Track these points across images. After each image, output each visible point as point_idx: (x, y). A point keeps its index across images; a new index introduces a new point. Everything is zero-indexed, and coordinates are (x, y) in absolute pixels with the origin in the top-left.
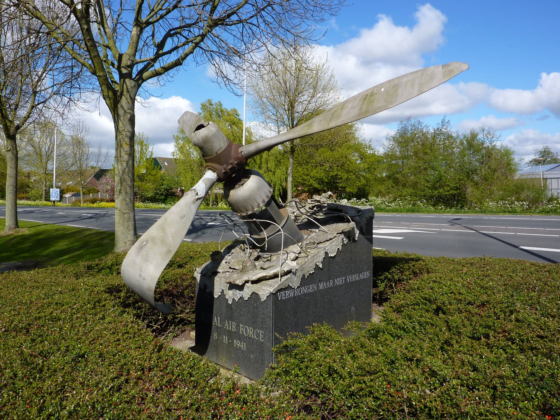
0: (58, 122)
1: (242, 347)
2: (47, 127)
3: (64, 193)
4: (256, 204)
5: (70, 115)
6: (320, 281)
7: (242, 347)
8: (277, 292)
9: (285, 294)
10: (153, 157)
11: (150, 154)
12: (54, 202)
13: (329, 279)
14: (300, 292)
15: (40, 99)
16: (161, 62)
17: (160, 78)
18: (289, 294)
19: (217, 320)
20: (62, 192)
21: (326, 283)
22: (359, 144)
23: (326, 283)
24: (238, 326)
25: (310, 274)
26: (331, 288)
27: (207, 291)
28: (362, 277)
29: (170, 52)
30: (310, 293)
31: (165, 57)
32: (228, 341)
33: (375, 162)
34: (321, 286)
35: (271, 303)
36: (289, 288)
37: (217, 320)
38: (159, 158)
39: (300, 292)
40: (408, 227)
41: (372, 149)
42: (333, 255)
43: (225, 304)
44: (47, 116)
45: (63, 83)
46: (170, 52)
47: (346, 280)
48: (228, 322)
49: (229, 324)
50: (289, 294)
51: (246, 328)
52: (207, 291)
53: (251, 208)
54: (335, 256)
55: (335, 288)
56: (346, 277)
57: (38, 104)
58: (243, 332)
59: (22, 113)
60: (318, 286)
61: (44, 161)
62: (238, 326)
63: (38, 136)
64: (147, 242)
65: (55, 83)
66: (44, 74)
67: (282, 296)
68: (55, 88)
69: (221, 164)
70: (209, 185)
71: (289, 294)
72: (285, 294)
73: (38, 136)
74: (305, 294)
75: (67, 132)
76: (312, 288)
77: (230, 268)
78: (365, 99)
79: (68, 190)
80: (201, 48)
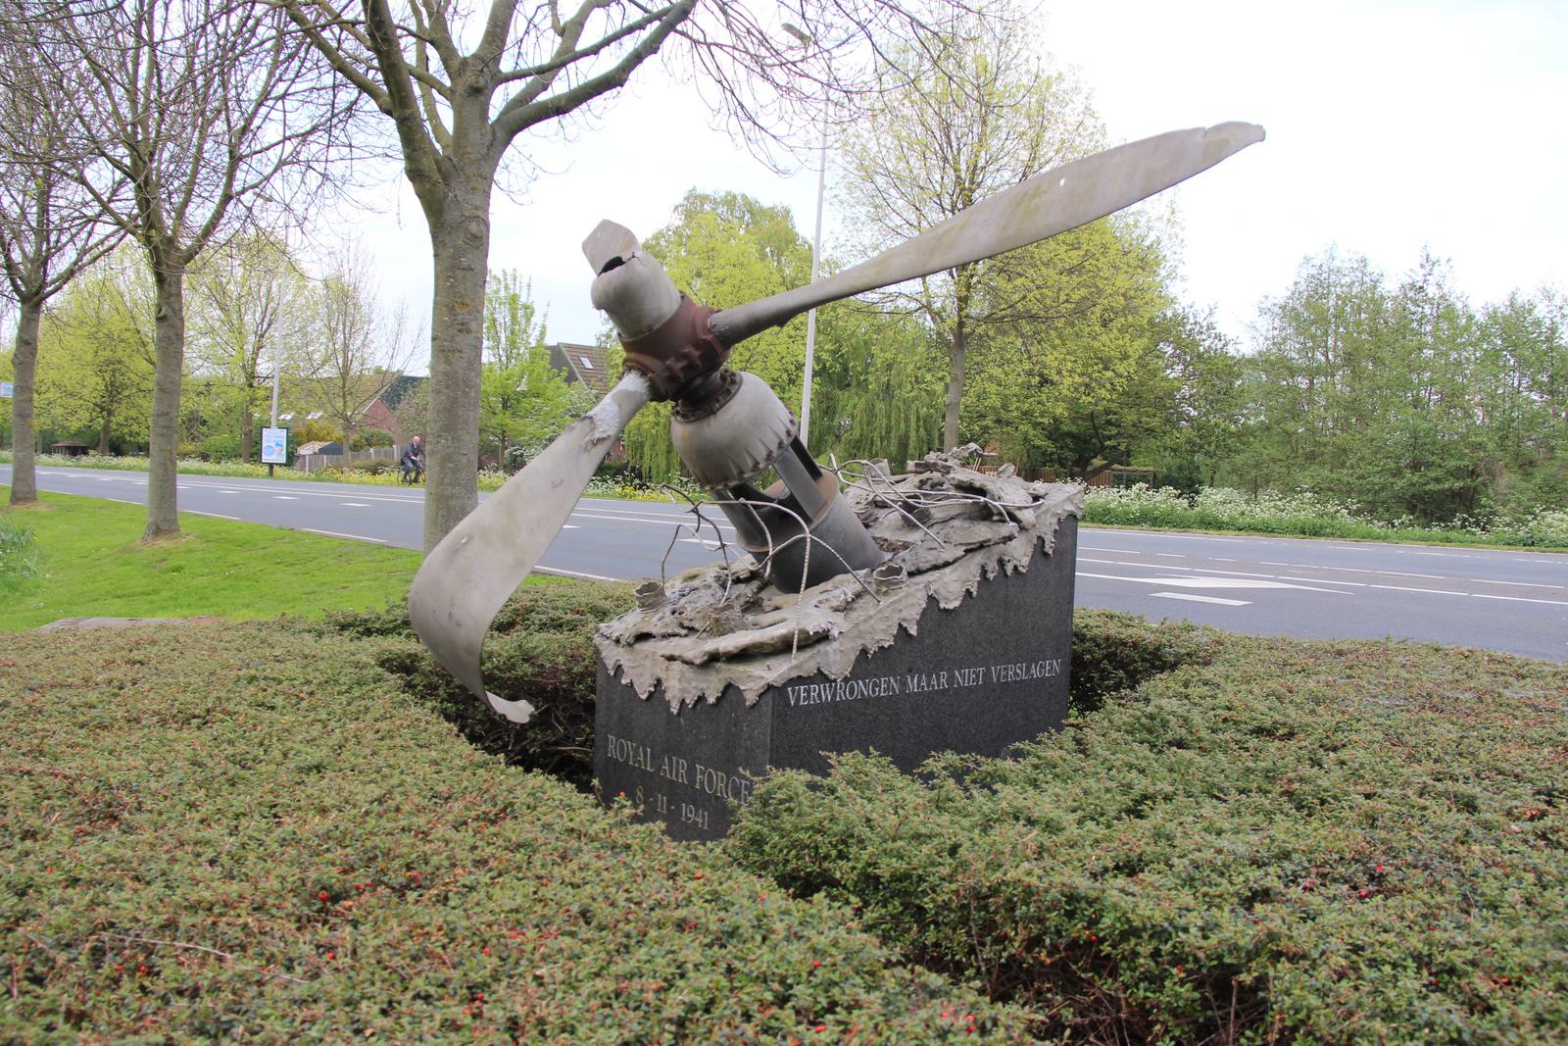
0: (291, 241)
1: (700, 820)
2: (266, 252)
3: (299, 445)
4: (750, 463)
5: (321, 223)
6: (910, 671)
7: (700, 820)
8: (785, 685)
9: (808, 691)
10: (551, 340)
11: (537, 333)
12: (271, 465)
13: (937, 668)
14: (852, 692)
15: (249, 178)
16: (572, 73)
17: (566, 119)
18: (819, 695)
19: (645, 755)
20: (293, 443)
21: (929, 677)
22: (1179, 321)
23: (929, 677)
24: (691, 770)
25: (882, 647)
26: (943, 692)
27: (624, 682)
28: (1035, 672)
29: (595, 51)
30: (879, 698)
31: (584, 63)
32: (668, 809)
33: (1218, 372)
34: (913, 684)
35: (767, 708)
36: (821, 677)
37: (645, 755)
38: (569, 347)
39: (852, 692)
40: (1276, 573)
41: (1218, 337)
42: (951, 606)
43: (664, 715)
44: (263, 224)
45: (310, 133)
46: (595, 51)
47: (987, 674)
48: (670, 760)
49: (671, 766)
50: (820, 693)
51: (710, 774)
52: (624, 682)
53: (735, 472)
54: (954, 610)
55: (956, 693)
56: (989, 669)
57: (243, 191)
58: (702, 783)
59: (199, 214)
60: (903, 684)
61: (249, 347)
62: (691, 770)
63: (235, 272)
64: (471, 538)
65: (288, 134)
66: (263, 110)
67: (800, 696)
68: (289, 146)
69: (662, 357)
70: (628, 407)
71: (819, 695)
72: (808, 691)
73: (235, 272)
74: (865, 701)
75: (315, 267)
76: (885, 686)
77: (682, 626)
78: (1019, 204)
79: (311, 436)
80: (683, 34)
